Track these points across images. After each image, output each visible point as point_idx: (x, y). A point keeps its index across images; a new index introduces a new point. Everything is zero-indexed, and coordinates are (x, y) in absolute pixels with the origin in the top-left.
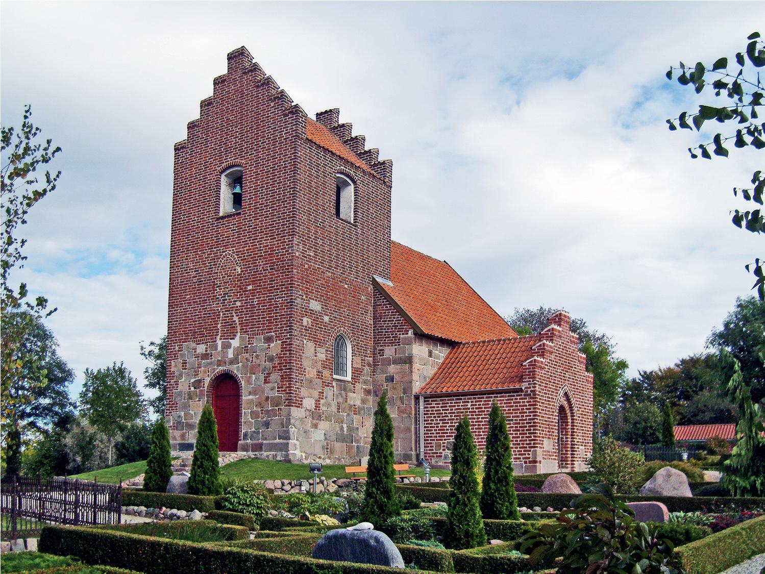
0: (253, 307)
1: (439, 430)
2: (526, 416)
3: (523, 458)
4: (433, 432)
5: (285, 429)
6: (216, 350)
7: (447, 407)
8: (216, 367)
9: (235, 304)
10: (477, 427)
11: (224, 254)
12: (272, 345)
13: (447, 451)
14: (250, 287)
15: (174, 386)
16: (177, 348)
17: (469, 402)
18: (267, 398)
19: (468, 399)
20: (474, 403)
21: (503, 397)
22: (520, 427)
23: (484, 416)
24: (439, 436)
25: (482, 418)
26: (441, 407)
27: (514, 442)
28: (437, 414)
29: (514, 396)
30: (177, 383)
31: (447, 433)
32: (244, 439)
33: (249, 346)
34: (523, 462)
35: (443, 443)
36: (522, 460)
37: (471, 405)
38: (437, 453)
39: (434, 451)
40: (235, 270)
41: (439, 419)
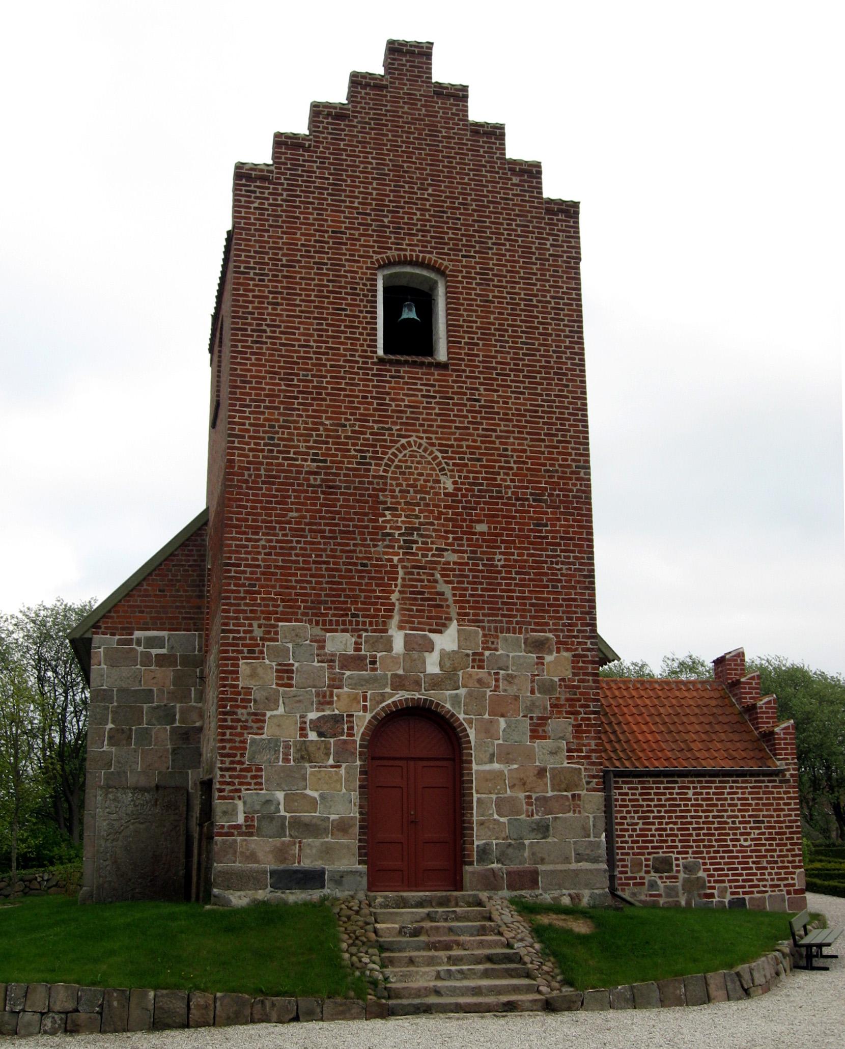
0: (491, 568)
1: (638, 836)
2: (785, 816)
3: (785, 886)
4: (627, 838)
5: (592, 839)
6: (389, 649)
7: (650, 794)
8: (388, 690)
9: (442, 556)
10: (705, 831)
11: (403, 441)
12: (548, 658)
13: (653, 874)
14: (481, 528)
15: (250, 724)
16: (258, 632)
17: (688, 788)
18: (541, 772)
19: (689, 782)
20: (698, 790)
21: (746, 782)
22: (777, 833)
23: (716, 814)
24: (638, 848)
25: (714, 817)
26: (641, 794)
27: (769, 859)
28: (633, 806)
29: (763, 782)
30: (259, 718)
31: (652, 842)
32: (481, 860)
33: (487, 653)
34: (784, 893)
35: (646, 860)
36: (782, 888)
37: (694, 794)
38: (635, 878)
39: (629, 874)
40: (439, 482)
41: (636, 816)
